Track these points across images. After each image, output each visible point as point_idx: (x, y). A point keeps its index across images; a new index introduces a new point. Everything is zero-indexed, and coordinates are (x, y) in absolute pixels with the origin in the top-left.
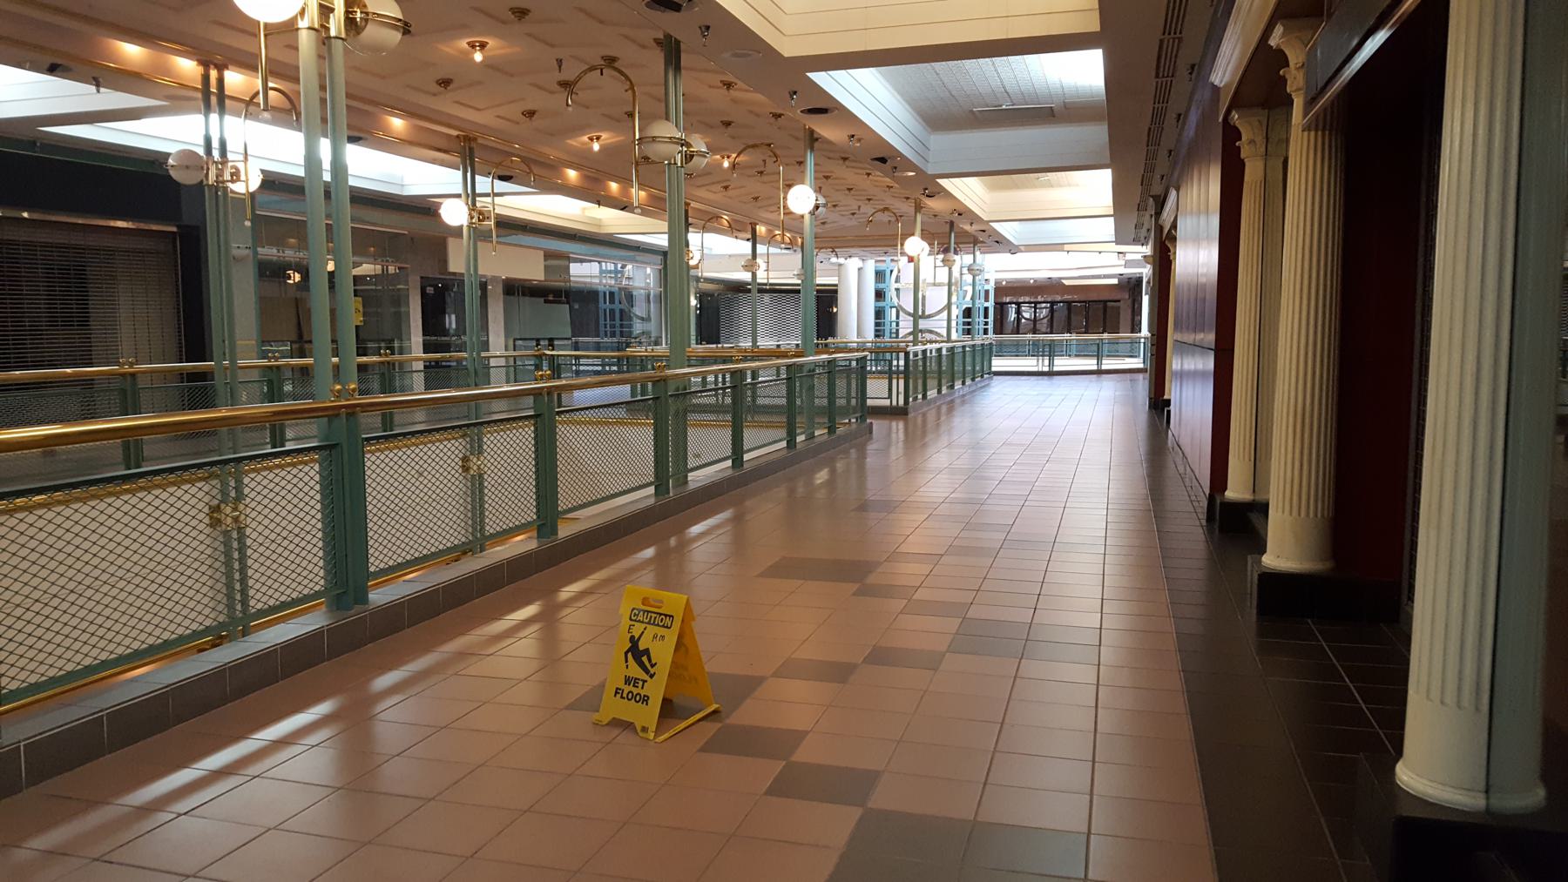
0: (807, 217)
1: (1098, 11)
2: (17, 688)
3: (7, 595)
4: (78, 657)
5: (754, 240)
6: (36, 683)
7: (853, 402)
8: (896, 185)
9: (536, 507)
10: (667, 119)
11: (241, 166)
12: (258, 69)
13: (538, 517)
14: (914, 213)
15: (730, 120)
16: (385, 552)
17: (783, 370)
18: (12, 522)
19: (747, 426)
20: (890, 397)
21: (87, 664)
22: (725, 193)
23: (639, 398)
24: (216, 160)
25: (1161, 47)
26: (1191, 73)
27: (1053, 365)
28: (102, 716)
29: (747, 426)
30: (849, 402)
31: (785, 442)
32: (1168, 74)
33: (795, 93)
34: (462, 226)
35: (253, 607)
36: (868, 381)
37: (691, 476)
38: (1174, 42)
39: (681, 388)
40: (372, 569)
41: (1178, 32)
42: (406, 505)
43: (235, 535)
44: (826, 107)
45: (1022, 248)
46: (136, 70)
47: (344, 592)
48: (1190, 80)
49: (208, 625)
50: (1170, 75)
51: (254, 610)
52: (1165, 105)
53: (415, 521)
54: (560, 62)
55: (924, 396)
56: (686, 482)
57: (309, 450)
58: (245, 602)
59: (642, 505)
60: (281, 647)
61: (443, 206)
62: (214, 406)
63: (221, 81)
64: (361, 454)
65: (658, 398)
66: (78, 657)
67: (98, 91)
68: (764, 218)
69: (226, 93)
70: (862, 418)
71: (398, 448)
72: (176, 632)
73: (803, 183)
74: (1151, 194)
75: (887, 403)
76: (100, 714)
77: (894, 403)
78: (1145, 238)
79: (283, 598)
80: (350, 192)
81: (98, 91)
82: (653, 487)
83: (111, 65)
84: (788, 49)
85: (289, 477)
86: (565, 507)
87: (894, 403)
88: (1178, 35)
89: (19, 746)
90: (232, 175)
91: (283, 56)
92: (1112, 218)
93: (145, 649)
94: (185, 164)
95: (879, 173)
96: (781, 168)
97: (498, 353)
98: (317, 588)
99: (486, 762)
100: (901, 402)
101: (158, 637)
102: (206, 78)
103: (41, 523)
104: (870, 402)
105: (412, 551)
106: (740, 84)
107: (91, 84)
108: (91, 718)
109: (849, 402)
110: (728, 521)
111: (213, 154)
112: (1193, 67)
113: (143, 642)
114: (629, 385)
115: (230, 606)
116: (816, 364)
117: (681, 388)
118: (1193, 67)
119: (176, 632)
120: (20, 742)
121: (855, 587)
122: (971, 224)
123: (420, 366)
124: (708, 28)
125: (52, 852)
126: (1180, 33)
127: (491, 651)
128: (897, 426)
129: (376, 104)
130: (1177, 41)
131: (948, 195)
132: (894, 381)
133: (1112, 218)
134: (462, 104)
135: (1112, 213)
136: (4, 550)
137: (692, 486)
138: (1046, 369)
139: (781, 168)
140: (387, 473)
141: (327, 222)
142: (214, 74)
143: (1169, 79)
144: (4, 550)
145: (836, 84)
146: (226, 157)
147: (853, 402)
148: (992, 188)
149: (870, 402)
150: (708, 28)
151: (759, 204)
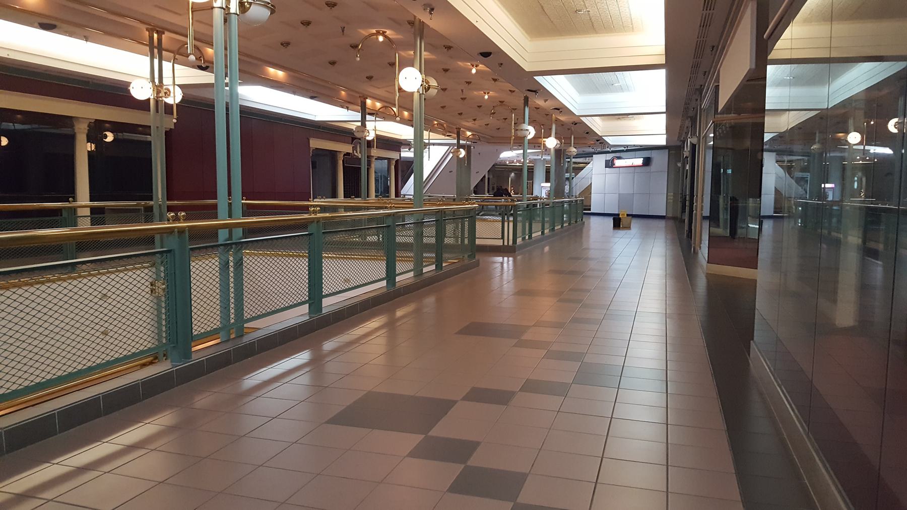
0: (416, 96)
2: (50, 379)
3: (5, 338)
4: (54, 371)
5: (364, 111)
6: (15, 390)
7: (466, 241)
8: (516, 90)
11: (171, 88)
12: (188, 37)
13: (309, 298)
14: (523, 106)
15: (447, 68)
16: (303, 296)
18: (8, 293)
19: (398, 260)
20: (503, 238)
21: (38, 381)
22: (473, 122)
24: (156, 84)
26: (712, 51)
29: (398, 260)
30: (463, 241)
34: (149, 99)
36: (325, 263)
37: (398, 279)
39: (420, 219)
44: (538, 90)
46: (33, 10)
47: (313, 303)
49: (79, 369)
52: (711, 11)
53: (287, 286)
54: (462, 91)
55: (530, 237)
56: (321, 309)
57: (433, 221)
59: (409, 281)
60: (58, 412)
61: (132, 85)
63: (160, 40)
65: (438, 220)
66: (54, 371)
68: (465, 125)
69: (367, 107)
70: (472, 256)
71: (199, 260)
72: (45, 378)
73: (413, 66)
74: (689, 115)
75: (500, 243)
76: (53, 412)
77: (506, 244)
80: (240, 108)
82: (386, 281)
83: (17, 7)
84: (527, 67)
85: (204, 265)
86: (327, 293)
87: (506, 244)
90: (166, 93)
91: (202, 29)
92: (665, 115)
95: (502, 80)
96: (513, 115)
97: (83, 203)
100: (511, 243)
102: (151, 38)
103: (38, 292)
104: (478, 242)
105: (256, 311)
106: (501, 79)
107: (83, 40)
109: (463, 241)
110: (170, 429)
111: (155, 81)
112: (713, 47)
117: (420, 219)
118: (713, 47)
119: (45, 378)
121: (515, 341)
122: (546, 101)
123: (87, 212)
124: (502, 64)
125: (83, 468)
127: (346, 350)
128: (508, 261)
129: (260, 60)
131: (548, 95)
132: (506, 224)
133: (665, 115)
134: (160, 8)
135: (665, 111)
136: (3, 311)
137: (195, 358)
139: (513, 115)
140: (256, 265)
142: (155, 36)
144: (3, 311)
145: (548, 83)
146: (162, 83)
147: (466, 241)
148: (603, 120)
149: (478, 242)
150: (502, 64)
151: (462, 116)
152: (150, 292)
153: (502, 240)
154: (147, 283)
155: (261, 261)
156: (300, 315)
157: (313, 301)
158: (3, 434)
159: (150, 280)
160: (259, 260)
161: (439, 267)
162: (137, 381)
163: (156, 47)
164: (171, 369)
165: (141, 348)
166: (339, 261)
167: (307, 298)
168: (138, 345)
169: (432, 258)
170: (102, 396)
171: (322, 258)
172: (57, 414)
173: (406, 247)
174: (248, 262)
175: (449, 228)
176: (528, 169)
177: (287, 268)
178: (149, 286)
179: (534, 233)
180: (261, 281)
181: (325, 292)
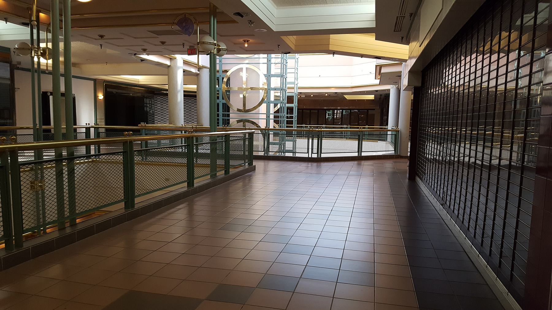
1: (375, 21)
9: (187, 176)
10: (210, 36)
17: (247, 135)
20: (308, 152)
23: (183, 144)
25: (397, 19)
27: (321, 153)
28: (94, 225)
30: (244, 153)
31: (224, 171)
32: (398, 30)
33: (279, 45)
35: (66, 215)
37: (137, 200)
38: (398, 30)
40: (77, 212)
41: (402, 14)
42: (81, 188)
43: (40, 192)
45: (291, 41)
48: (410, 20)
49: (86, 210)
50: (399, 31)
51: (66, 216)
58: (44, 217)
62: (141, 135)
64: (133, 156)
67: (6, 23)
78: (411, 15)
79: (109, 202)
81: (6, 23)
88: (403, 15)
89: (30, 248)
93: (52, 221)
94: (22, 47)
98: (54, 219)
99: (153, 275)
101: (51, 219)
108: (5, 256)
109: (244, 153)
113: (96, 206)
114: (85, 146)
115: (38, 218)
116: (219, 136)
120: (29, 247)
126: (404, 15)
130: (403, 17)
138: (315, 156)
141: (218, 95)
143: (401, 15)
152: (30, 188)
153: (308, 154)
154: (28, 182)
155: (147, 168)
156: (183, 187)
157: (128, 200)
158: (30, 249)
159: (30, 179)
160: (146, 167)
161: (227, 172)
162: (53, 239)
163: (62, 75)
164: (5, 255)
165: (86, 209)
166: (199, 168)
167: (123, 198)
168: (100, 203)
169: (538, 93)
170: (31, 248)
171: (513, 145)
172: (3, 259)
173: (488, 147)
174: (137, 169)
175: (92, 147)
176: (217, 97)
177: (159, 173)
178: (30, 184)
179: (139, 196)
180: (146, 179)
181: (195, 176)
